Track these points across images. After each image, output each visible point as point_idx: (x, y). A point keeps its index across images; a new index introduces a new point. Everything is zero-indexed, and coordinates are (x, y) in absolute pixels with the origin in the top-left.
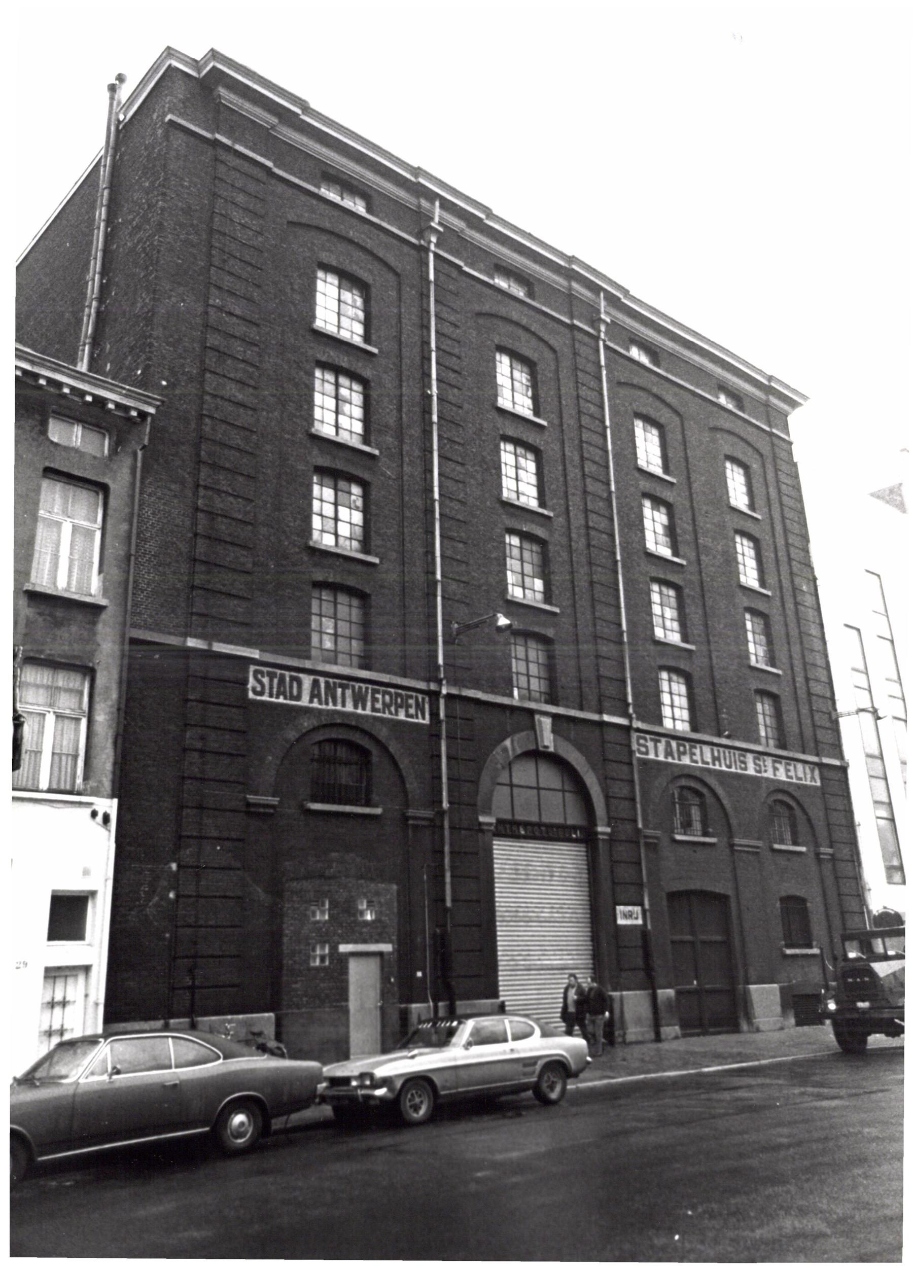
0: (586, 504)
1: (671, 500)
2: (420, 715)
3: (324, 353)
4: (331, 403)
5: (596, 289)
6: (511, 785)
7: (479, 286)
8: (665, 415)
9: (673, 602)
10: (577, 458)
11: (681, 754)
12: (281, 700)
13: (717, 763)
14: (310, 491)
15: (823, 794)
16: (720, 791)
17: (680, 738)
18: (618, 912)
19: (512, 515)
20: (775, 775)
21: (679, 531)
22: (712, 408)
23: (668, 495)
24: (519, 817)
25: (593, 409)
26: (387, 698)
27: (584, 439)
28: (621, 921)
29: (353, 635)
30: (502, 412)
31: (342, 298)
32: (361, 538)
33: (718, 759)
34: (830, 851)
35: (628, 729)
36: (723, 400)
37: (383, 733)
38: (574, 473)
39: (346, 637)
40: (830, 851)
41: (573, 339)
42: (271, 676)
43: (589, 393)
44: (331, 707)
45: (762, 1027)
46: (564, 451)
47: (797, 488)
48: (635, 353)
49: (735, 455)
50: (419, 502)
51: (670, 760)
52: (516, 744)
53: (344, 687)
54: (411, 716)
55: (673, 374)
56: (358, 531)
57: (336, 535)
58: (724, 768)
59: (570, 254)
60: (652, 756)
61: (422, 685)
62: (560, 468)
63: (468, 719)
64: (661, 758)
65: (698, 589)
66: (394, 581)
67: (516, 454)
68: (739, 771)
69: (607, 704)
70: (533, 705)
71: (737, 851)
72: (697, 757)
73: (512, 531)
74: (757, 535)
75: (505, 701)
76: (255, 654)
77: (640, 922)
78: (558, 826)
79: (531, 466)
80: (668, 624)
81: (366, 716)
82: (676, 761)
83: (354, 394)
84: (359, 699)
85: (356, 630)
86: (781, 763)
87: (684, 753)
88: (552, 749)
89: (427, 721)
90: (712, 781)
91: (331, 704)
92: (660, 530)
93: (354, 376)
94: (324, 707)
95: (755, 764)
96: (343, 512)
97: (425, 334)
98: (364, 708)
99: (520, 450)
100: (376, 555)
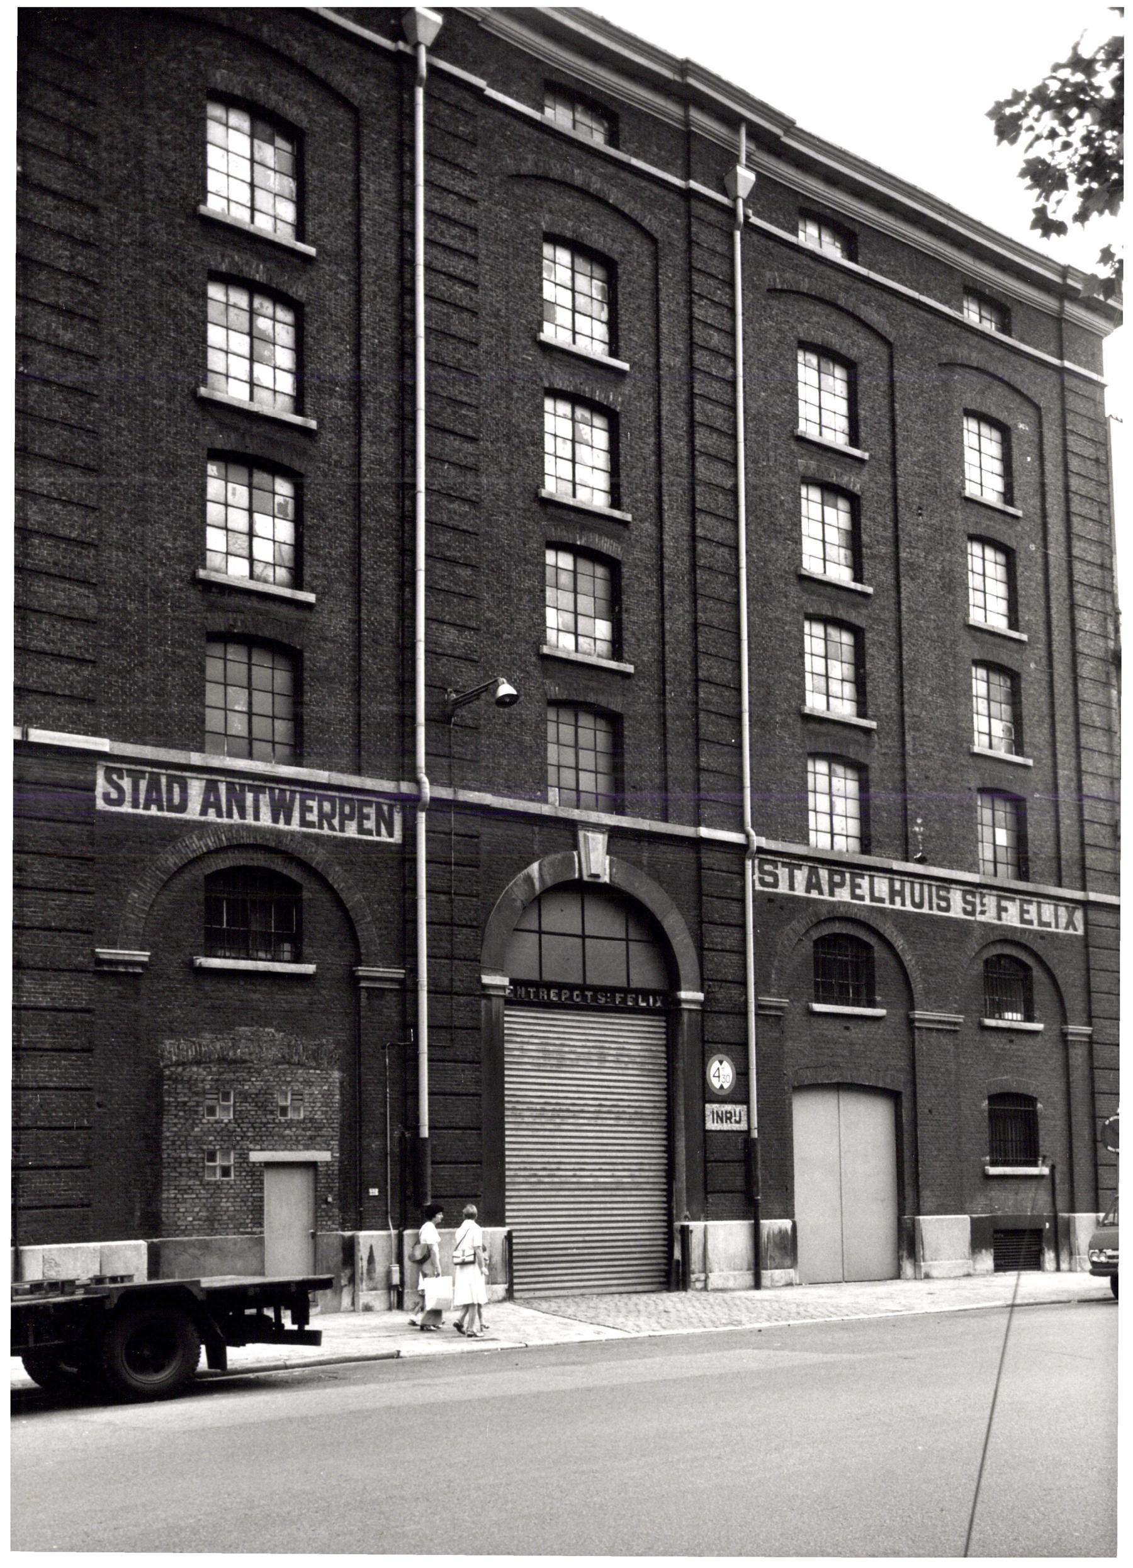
0: (693, 499)
1: (857, 489)
2: (383, 831)
3: (223, 256)
4: (240, 343)
5: (732, 121)
6: (540, 932)
7: (517, 124)
8: (859, 345)
9: (847, 653)
10: (682, 422)
11: (833, 886)
12: (154, 811)
13: (898, 899)
14: (203, 489)
15: (1087, 946)
16: (899, 943)
17: (835, 865)
18: (708, 1112)
19: (560, 520)
20: (1000, 918)
21: (865, 538)
22: (952, 329)
23: (854, 482)
24: (548, 977)
25: (716, 339)
26: (327, 807)
27: (696, 391)
28: (711, 1125)
29: (277, 713)
30: (802, 440)
31: (257, 157)
32: (290, 564)
33: (901, 894)
34: (1087, 1030)
35: (742, 850)
36: (972, 314)
37: (319, 857)
38: (674, 446)
39: (268, 717)
40: (1087, 1030)
41: (689, 214)
42: (136, 777)
43: (712, 311)
44: (236, 819)
45: (934, 1273)
46: (659, 411)
47: (1103, 463)
48: (809, 236)
49: (984, 410)
50: (388, 503)
51: (814, 894)
52: (545, 869)
53: (257, 790)
54: (369, 832)
55: (881, 272)
56: (287, 552)
57: (251, 559)
58: (909, 908)
59: (680, 54)
60: (783, 888)
61: (388, 786)
62: (652, 440)
63: (472, 837)
64: (800, 891)
65: (892, 633)
66: (344, 628)
67: (573, 420)
68: (935, 912)
69: (706, 813)
70: (576, 814)
71: (919, 1028)
72: (864, 890)
73: (559, 546)
74: (1012, 543)
75: (533, 808)
76: (103, 744)
77: (743, 1126)
78: (614, 990)
79: (601, 439)
80: (835, 687)
81: (292, 834)
82: (826, 897)
83: (279, 326)
84: (281, 809)
85: (283, 706)
86: (1013, 900)
87: (841, 885)
88: (606, 879)
89: (397, 838)
90: (889, 930)
91: (236, 816)
92: (834, 536)
93: (280, 298)
94: (225, 820)
95: (966, 902)
96: (263, 523)
97: (407, 218)
98: (288, 821)
99: (581, 413)
100: (313, 590)
